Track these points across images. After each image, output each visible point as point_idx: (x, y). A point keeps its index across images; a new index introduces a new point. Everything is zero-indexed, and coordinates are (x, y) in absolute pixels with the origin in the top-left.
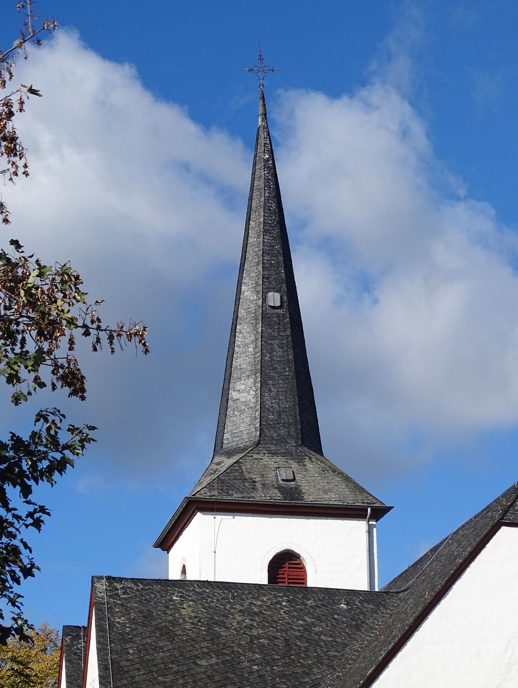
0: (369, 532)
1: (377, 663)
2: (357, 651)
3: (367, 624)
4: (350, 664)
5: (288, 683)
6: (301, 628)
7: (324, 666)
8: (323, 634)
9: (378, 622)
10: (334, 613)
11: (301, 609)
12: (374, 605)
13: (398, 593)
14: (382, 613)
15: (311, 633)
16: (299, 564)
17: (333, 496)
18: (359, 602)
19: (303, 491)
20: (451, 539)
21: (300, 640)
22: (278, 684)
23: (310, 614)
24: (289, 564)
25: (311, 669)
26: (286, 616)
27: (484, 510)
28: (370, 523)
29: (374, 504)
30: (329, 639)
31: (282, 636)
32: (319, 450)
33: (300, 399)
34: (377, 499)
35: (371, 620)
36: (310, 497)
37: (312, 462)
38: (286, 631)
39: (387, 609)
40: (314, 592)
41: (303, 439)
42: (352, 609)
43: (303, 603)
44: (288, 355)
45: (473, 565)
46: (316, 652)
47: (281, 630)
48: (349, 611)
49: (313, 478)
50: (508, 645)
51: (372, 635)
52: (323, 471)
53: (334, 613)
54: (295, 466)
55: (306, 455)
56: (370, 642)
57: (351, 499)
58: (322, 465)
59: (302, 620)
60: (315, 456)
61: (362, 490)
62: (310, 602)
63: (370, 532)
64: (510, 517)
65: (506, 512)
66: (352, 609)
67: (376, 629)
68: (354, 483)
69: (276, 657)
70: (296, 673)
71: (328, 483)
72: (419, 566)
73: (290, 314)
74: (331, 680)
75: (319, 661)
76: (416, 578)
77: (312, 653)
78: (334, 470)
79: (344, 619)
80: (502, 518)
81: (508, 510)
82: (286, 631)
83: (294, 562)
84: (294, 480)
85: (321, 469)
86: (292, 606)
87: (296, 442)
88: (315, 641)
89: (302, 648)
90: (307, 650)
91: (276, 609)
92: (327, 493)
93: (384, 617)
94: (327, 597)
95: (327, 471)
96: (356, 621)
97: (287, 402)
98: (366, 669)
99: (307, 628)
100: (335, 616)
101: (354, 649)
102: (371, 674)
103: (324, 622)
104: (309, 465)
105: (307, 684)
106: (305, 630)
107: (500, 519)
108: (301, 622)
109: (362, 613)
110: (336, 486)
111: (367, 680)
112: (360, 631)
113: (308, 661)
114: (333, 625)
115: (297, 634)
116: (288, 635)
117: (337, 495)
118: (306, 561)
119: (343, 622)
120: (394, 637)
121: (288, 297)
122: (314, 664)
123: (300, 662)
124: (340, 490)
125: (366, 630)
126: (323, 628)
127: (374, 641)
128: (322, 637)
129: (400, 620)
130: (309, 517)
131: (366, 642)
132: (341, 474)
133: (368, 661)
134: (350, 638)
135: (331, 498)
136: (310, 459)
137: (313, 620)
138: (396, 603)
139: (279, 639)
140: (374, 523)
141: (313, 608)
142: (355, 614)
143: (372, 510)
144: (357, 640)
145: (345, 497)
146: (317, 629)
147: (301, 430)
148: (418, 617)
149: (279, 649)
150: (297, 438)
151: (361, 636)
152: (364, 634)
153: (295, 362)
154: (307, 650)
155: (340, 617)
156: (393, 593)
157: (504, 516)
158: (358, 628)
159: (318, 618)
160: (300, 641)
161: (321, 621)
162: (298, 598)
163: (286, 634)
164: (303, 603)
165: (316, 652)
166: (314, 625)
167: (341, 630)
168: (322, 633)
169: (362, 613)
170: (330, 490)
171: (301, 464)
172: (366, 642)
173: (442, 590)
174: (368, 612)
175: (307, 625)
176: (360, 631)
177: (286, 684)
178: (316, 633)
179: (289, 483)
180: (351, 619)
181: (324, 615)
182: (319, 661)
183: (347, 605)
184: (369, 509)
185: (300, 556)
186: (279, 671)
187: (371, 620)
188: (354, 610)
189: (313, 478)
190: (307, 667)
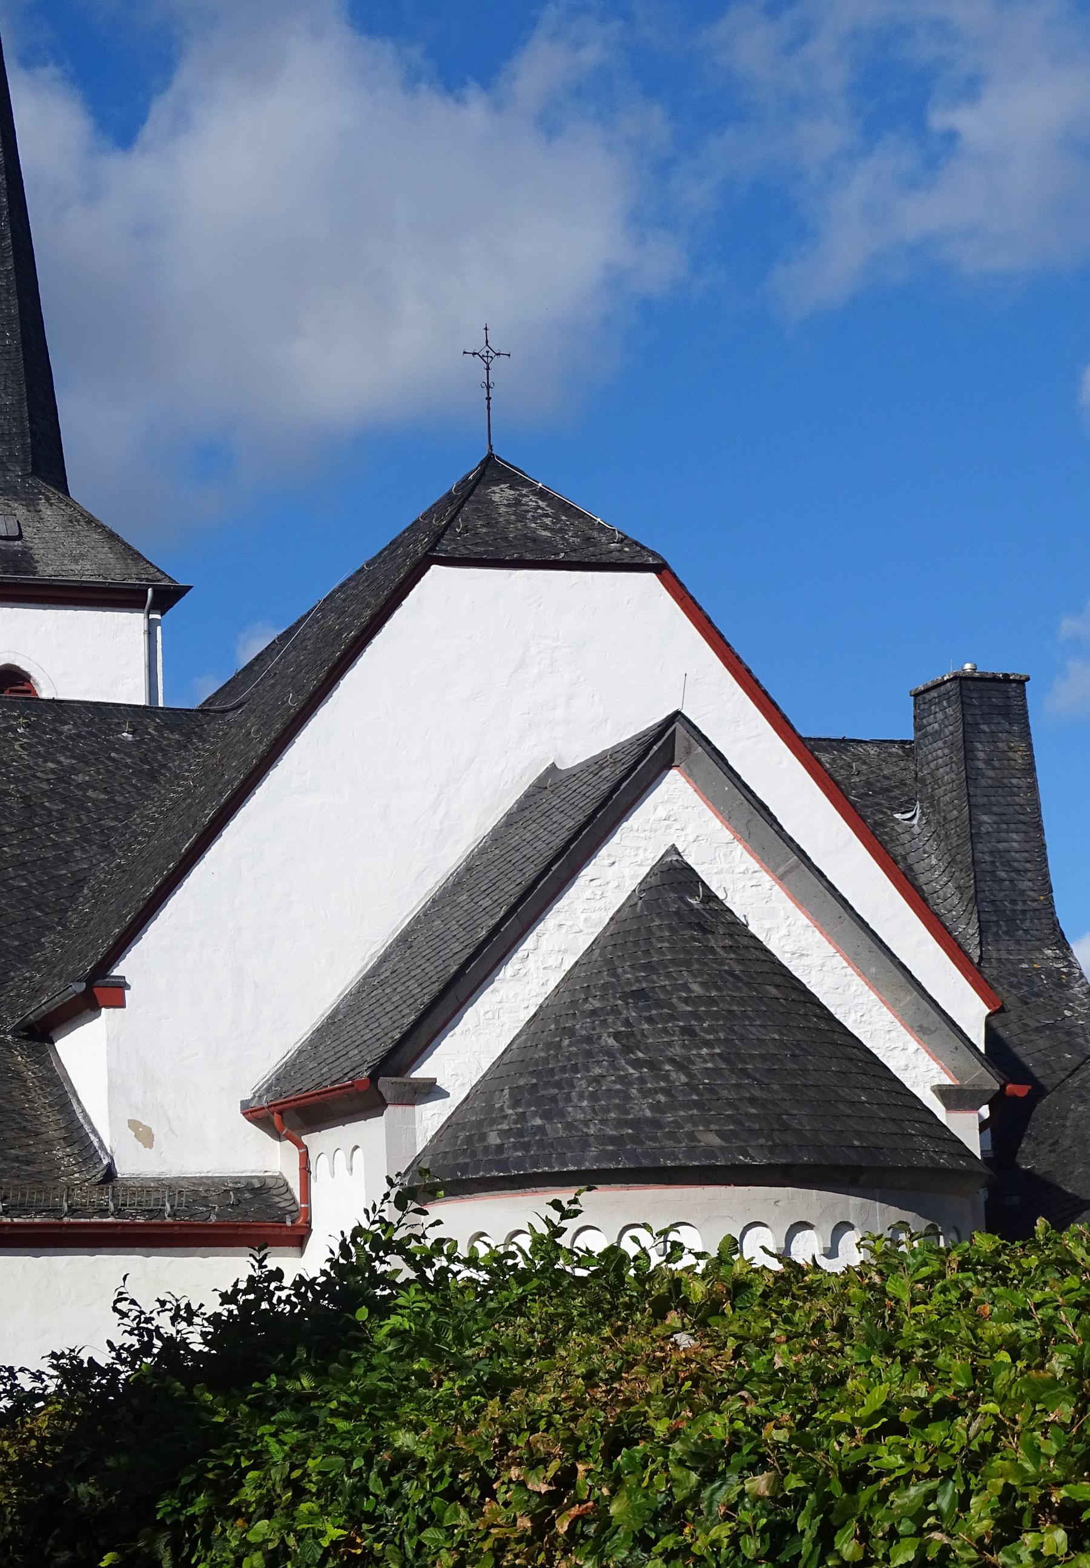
0: (149, 633)
1: (201, 829)
2: (153, 819)
3: (169, 769)
4: (140, 843)
5: (29, 877)
6: (51, 776)
7: (94, 847)
8: (91, 787)
9: (190, 765)
10: (109, 749)
11: (50, 741)
12: (182, 734)
13: (225, 711)
14: (197, 749)
15: (70, 784)
16: (28, 692)
17: (88, 567)
18: (156, 729)
19: (36, 557)
20: (321, 609)
21: (49, 797)
22: (11, 878)
23: (66, 748)
24: (12, 691)
25: (70, 852)
26: (24, 754)
27: (385, 549)
28: (152, 616)
29: (159, 581)
30: (103, 796)
31: (18, 791)
32: (60, 483)
33: (30, 389)
34: (163, 573)
35: (177, 763)
36: (50, 566)
37: (51, 505)
38: (25, 781)
39: (205, 741)
40: (74, 709)
41: (34, 464)
42: (142, 740)
43: (54, 730)
44: (9, 309)
45: (377, 640)
46: (79, 820)
47: (16, 780)
48: (137, 744)
49: (54, 535)
50: (439, 795)
51: (180, 789)
52: (71, 521)
53: (109, 749)
54: (21, 512)
55: (40, 493)
56: (176, 802)
57: (118, 573)
58: (69, 511)
59: (53, 762)
60: (55, 495)
61: (138, 557)
62: (66, 727)
63: (151, 634)
64: (447, 546)
65: (438, 537)
66: (142, 740)
67: (186, 779)
68: (124, 544)
69: (8, 829)
70: (45, 858)
71: (78, 543)
72: (256, 668)
73: (12, 231)
74: (107, 873)
75: (85, 837)
76: (256, 686)
77: (72, 823)
78: (90, 520)
79: (129, 760)
80: (433, 549)
81: (443, 534)
82: (25, 781)
83: (20, 688)
84: (20, 537)
85: (66, 518)
86: (34, 735)
87: (22, 470)
88: (78, 799)
89: (54, 813)
90: (62, 816)
91: (6, 741)
92: (77, 563)
93: (199, 756)
94: (96, 720)
95: (78, 521)
96: (149, 763)
97: (7, 394)
98: (177, 843)
99: (63, 776)
100: (113, 754)
101: (146, 816)
102: (190, 851)
103: (93, 765)
104: (47, 512)
105: (64, 880)
106: (60, 779)
107: (429, 551)
108: (51, 765)
109: (160, 748)
110: (93, 548)
111: (181, 862)
112: (157, 782)
113: (64, 837)
114: (108, 771)
115: (45, 786)
116: (28, 789)
117: (93, 565)
118: (42, 686)
119: (127, 766)
120: (229, 782)
121: (8, 200)
122: (75, 842)
123: (51, 839)
124: (100, 556)
125: (169, 781)
126: (90, 775)
127: (184, 800)
128: (90, 793)
129: (236, 753)
130: (47, 606)
131: (168, 803)
132: (100, 527)
133: (178, 832)
134: (139, 795)
135: (85, 571)
136: (48, 499)
137: (74, 762)
138: (222, 730)
139: (12, 795)
140: (158, 617)
141: (73, 740)
142: (149, 751)
143: (154, 592)
144: (152, 799)
145: (108, 569)
146: (80, 778)
147: (32, 446)
148: (277, 740)
149: (13, 815)
150: (25, 461)
151: (159, 792)
152: (164, 788)
153: (21, 321)
154: (62, 816)
155: (122, 756)
156: (215, 711)
157: (436, 545)
158: (153, 776)
159: (81, 758)
160: (51, 800)
161: (87, 763)
162: (46, 720)
163: (25, 786)
164: (54, 730)
165: (79, 820)
166: (73, 770)
167: (123, 780)
168: (89, 785)
169: (160, 748)
170: (82, 556)
171: (32, 508)
172: (168, 803)
173: (320, 688)
174: (171, 746)
175: (62, 770)
176: (157, 782)
177: (26, 880)
178: (79, 786)
179: (11, 543)
180: (141, 760)
181: (92, 753)
182: (85, 837)
183: (133, 733)
184: (150, 590)
185: (30, 677)
186: (13, 855)
187: (177, 763)
188: (146, 743)
189: (54, 535)
190: (61, 849)
